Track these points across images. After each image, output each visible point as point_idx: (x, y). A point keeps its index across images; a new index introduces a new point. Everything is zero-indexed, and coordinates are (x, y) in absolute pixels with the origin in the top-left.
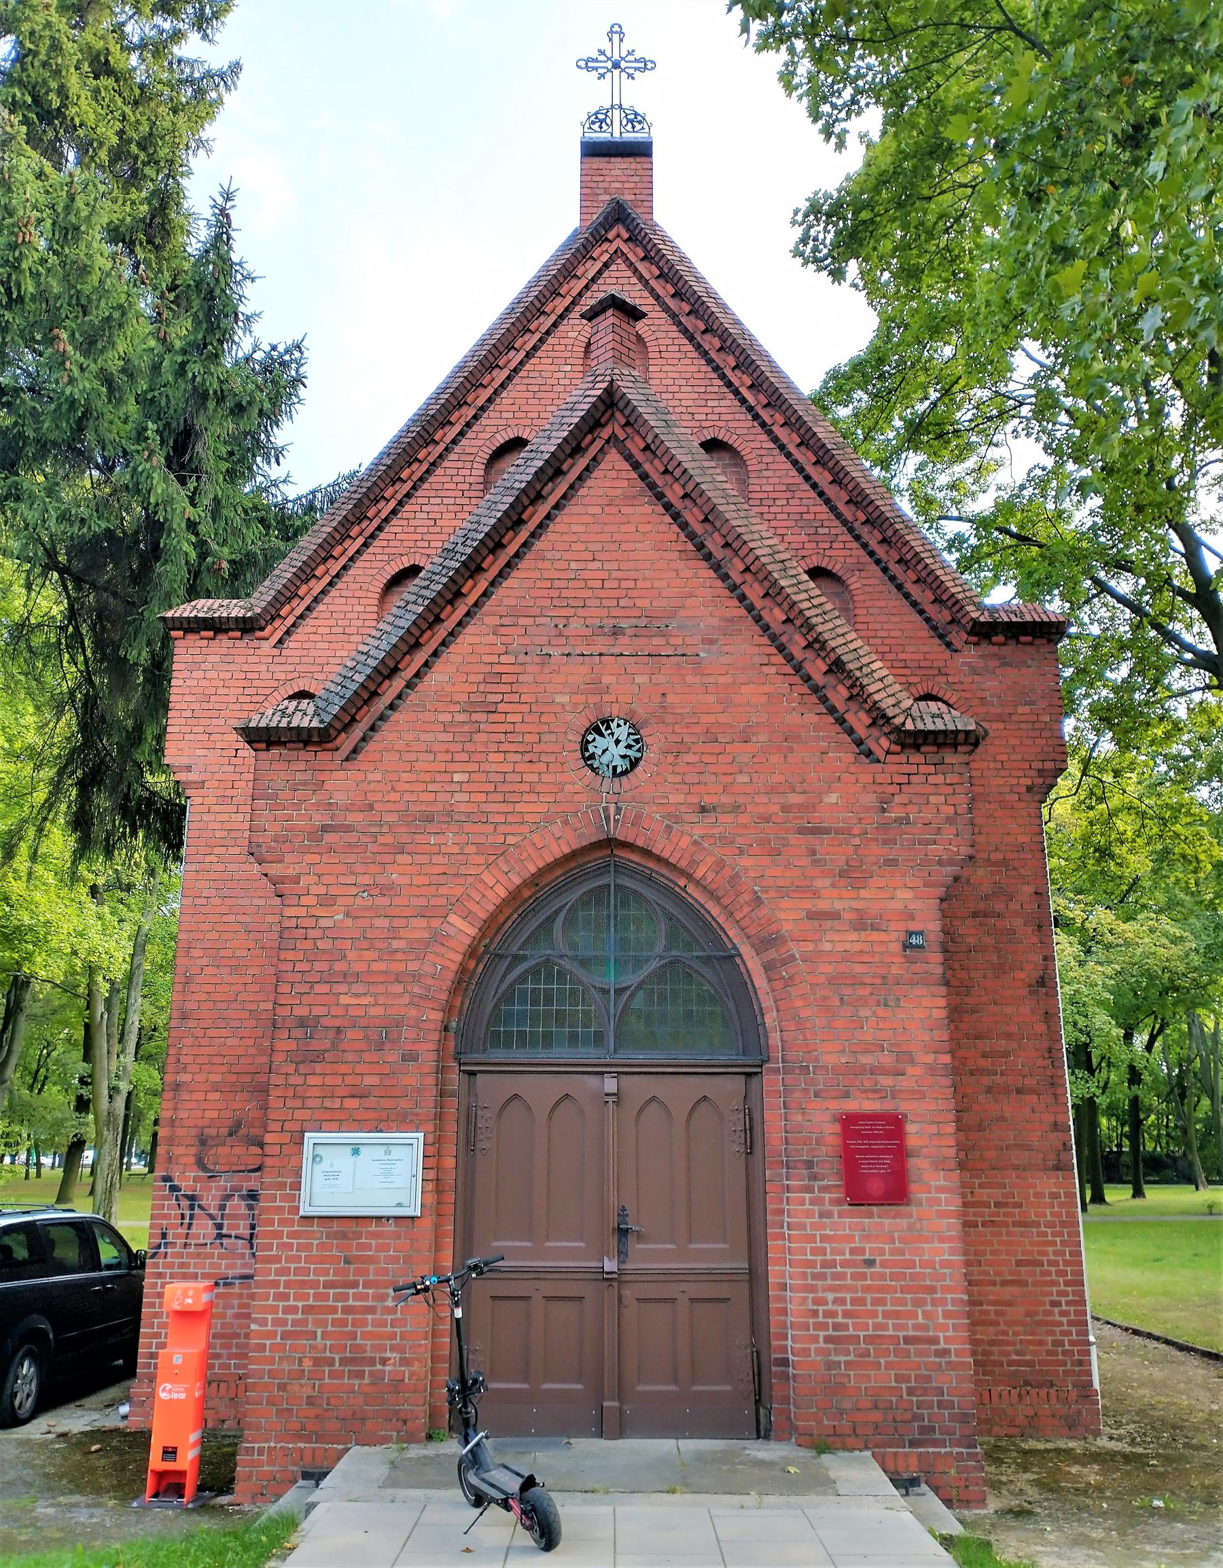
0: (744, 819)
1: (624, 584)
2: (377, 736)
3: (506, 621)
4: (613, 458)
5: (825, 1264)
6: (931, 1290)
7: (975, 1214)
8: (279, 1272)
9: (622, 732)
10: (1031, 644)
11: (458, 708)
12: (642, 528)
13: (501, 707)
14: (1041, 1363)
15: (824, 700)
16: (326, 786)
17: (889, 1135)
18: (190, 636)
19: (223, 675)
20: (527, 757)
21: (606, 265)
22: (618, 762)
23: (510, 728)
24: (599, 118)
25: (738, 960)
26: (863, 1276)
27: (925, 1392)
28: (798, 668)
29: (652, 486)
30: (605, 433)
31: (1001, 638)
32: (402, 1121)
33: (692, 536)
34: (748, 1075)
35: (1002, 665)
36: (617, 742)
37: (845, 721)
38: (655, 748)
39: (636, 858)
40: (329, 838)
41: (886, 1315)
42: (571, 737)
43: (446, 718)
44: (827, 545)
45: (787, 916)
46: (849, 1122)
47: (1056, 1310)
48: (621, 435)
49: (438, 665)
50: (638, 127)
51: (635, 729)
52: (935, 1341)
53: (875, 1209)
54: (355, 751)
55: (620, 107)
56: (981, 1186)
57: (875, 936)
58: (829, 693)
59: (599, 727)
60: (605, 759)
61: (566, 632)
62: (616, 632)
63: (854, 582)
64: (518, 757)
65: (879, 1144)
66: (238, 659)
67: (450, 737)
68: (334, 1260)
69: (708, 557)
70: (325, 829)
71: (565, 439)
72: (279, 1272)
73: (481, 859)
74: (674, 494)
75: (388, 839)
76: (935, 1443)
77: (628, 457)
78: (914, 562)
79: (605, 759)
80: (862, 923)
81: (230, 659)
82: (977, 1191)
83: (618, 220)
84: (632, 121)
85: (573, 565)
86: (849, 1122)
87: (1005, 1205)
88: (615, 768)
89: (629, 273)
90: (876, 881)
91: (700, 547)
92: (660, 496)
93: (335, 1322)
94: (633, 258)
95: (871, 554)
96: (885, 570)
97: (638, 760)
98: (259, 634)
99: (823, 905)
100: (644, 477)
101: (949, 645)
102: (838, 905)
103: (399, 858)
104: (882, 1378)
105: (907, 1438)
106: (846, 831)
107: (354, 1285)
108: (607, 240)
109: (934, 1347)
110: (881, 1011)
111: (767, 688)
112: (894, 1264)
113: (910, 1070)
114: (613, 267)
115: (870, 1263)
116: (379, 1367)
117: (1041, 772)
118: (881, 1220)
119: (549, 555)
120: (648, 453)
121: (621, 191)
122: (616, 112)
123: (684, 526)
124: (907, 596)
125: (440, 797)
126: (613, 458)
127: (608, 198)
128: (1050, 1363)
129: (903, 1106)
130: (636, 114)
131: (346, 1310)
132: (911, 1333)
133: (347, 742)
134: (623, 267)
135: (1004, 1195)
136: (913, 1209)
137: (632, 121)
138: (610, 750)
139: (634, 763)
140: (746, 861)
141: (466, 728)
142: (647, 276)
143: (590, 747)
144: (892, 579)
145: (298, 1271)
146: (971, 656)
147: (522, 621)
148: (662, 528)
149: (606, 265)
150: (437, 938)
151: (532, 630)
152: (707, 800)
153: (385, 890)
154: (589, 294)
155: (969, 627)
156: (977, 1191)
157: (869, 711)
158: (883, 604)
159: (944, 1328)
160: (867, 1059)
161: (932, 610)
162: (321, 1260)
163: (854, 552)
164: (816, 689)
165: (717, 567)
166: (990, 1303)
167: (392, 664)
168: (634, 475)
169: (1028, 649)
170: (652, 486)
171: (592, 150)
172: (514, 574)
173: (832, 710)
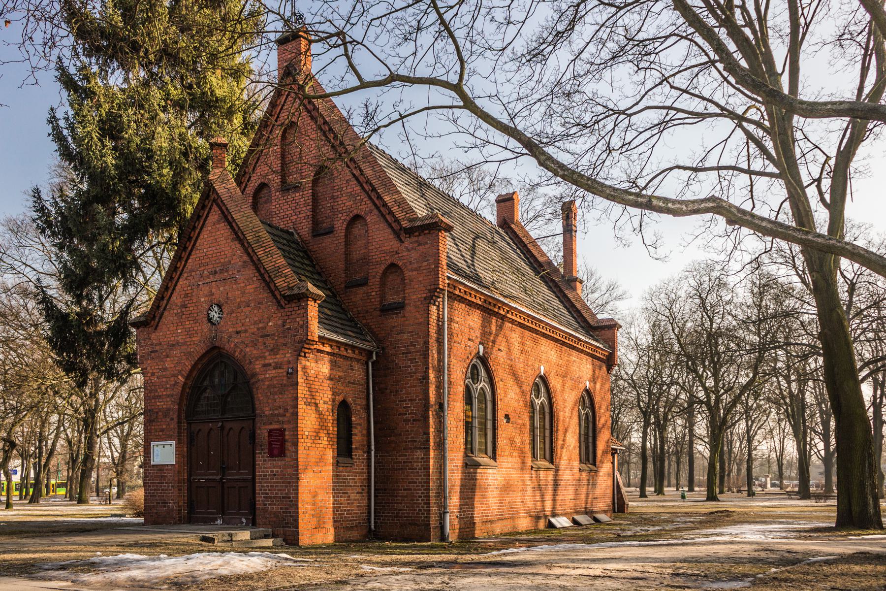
0: (247, 335)
6: (289, 483)
9: (216, 309)
31: (417, 234)
32: (168, 438)
40: (153, 355)
46: (270, 432)
62: (216, 272)
63: (368, 219)
70: (151, 352)
80: (277, 366)
86: (270, 432)
90: (281, 352)
99: (267, 362)
104: (276, 508)
106: (273, 335)
113: (288, 415)
115: (275, 475)
117: (430, 291)
140: (248, 349)
150: (176, 383)
152: (239, 329)
153: (165, 369)
160: (276, 412)
169: (429, 236)
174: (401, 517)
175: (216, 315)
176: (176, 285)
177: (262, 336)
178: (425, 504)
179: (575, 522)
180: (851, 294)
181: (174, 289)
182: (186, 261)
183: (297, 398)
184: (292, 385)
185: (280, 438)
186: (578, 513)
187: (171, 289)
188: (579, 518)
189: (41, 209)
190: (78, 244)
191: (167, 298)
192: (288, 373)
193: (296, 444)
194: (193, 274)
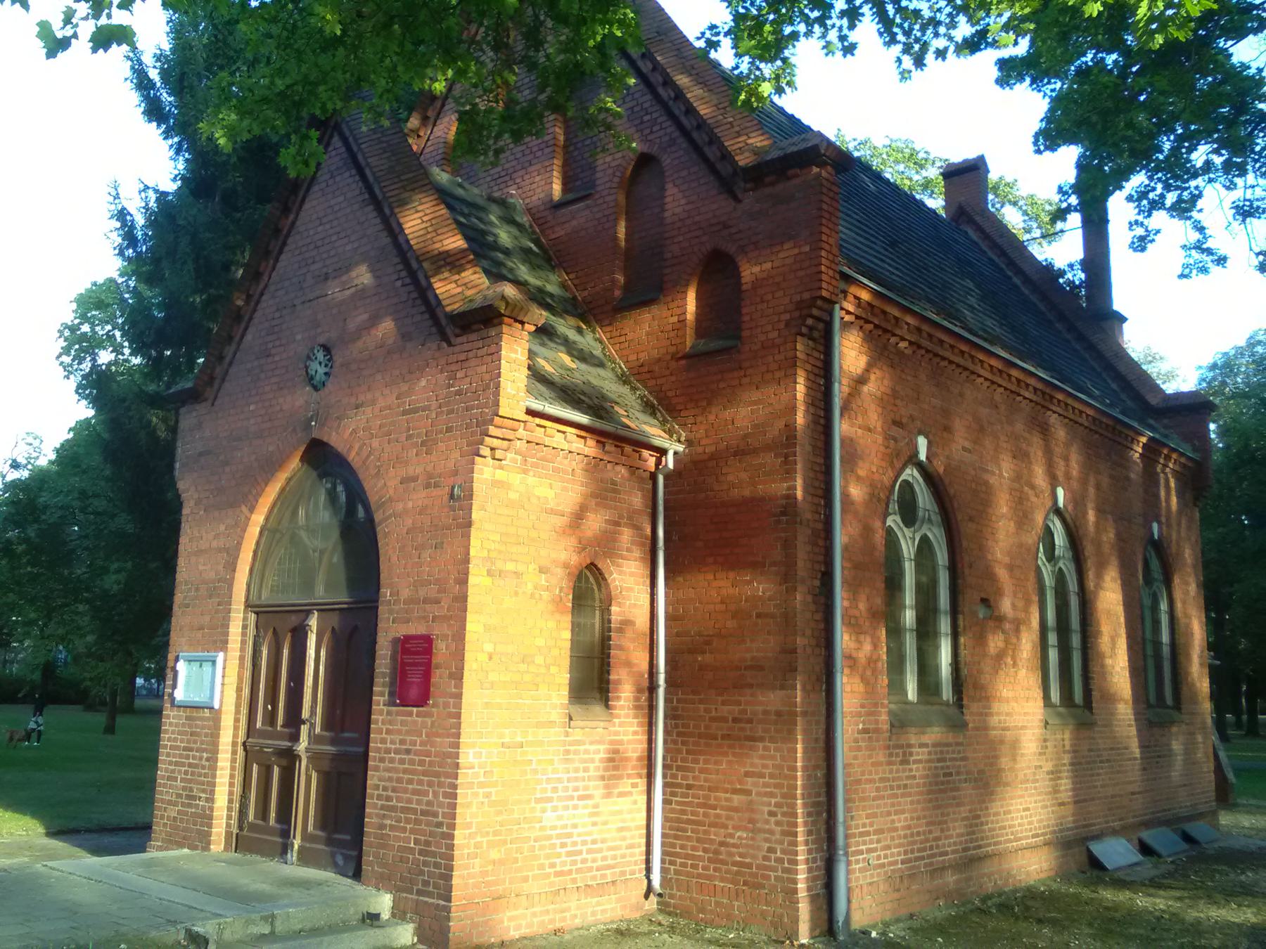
9: (320, 355)
47: (773, 819)
53: (415, 709)
56: (723, 703)
115: (408, 752)
166: (722, 808)
174: (723, 862)
176: (255, 310)
177: (405, 413)
178: (784, 833)
179: (1145, 849)
181: (251, 319)
183: (466, 560)
184: (459, 526)
186: (1147, 825)
187: (246, 318)
188: (1147, 835)
189: (122, 215)
191: (237, 339)
192: (452, 496)
193: (458, 676)
194: (287, 283)
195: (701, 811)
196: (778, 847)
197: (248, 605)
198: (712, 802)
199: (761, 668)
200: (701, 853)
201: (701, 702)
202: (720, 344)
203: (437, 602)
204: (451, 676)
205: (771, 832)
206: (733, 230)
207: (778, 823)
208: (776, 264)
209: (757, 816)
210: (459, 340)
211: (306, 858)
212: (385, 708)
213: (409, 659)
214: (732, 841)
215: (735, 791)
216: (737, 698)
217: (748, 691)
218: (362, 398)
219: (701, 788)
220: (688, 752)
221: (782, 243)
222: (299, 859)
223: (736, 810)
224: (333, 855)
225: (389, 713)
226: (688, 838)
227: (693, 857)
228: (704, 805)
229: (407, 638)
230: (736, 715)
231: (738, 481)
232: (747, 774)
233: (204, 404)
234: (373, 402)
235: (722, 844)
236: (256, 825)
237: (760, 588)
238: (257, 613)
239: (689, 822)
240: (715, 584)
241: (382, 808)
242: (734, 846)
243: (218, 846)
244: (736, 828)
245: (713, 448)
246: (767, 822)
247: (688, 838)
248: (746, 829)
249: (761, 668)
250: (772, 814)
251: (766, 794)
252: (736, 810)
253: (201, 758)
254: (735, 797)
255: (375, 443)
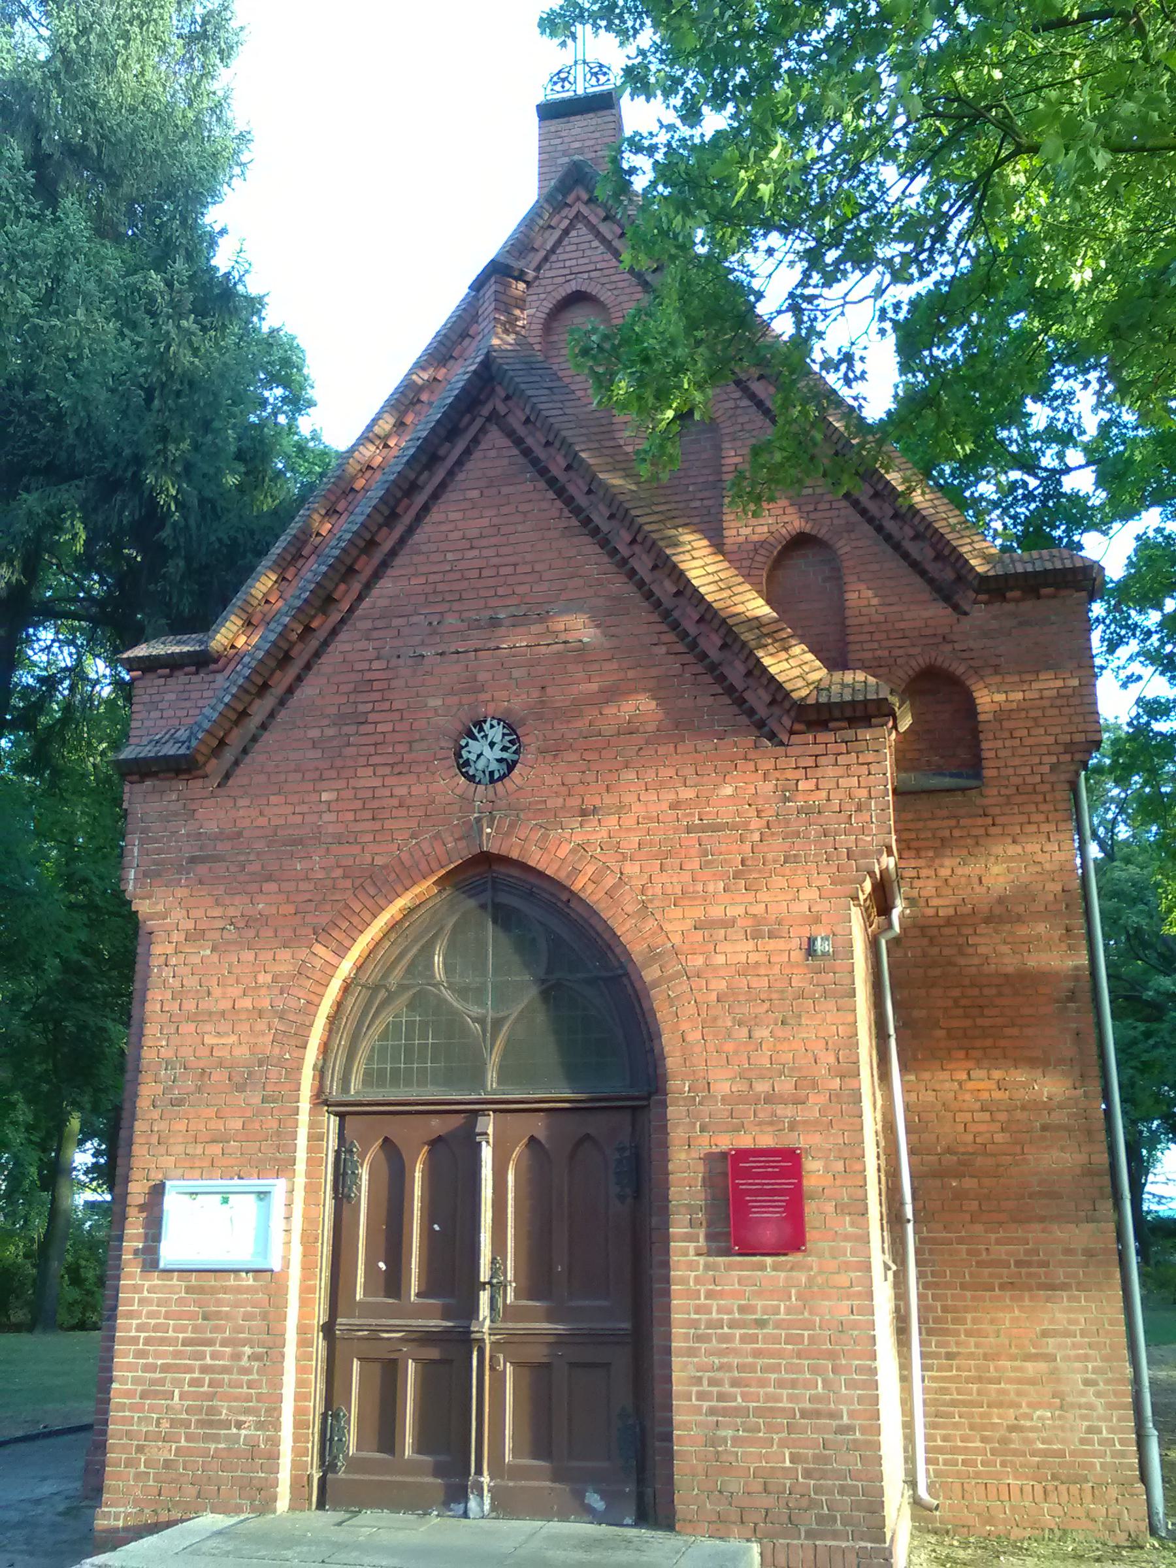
1: (503, 571)
2: (248, 759)
3: (379, 624)
4: (495, 437)
5: (710, 1324)
7: (991, 1275)
8: (139, 1329)
9: (496, 733)
10: (1054, 597)
11: (326, 722)
12: (523, 507)
13: (372, 717)
14: (1073, 1454)
15: (721, 678)
16: (197, 815)
17: (783, 1173)
18: (149, 676)
19: (180, 713)
20: (396, 770)
21: (566, 232)
22: (494, 766)
23: (380, 738)
24: (560, 78)
25: (625, 980)
26: (754, 1339)
27: (824, 1475)
28: (693, 646)
29: (535, 462)
30: (486, 411)
33: (577, 511)
34: (634, 1109)
35: (1020, 624)
36: (492, 745)
37: (745, 701)
38: (533, 748)
39: (515, 872)
41: (780, 1384)
42: (443, 744)
43: (314, 733)
44: (811, 508)
45: (678, 924)
47: (1091, 1390)
48: (502, 409)
49: (311, 677)
50: (603, 79)
51: (511, 728)
52: (834, 1415)
53: (769, 1260)
54: (227, 776)
55: (584, 62)
56: (998, 1242)
57: (772, 945)
58: (727, 671)
59: (474, 728)
60: (481, 765)
61: (442, 629)
63: (843, 547)
64: (387, 770)
65: (769, 1184)
66: (194, 695)
67: (319, 754)
68: (191, 1316)
69: (595, 532)
71: (438, 421)
72: (139, 1329)
73: (348, 883)
74: (557, 467)
75: (255, 867)
76: (835, 1535)
77: (510, 433)
78: (910, 515)
79: (481, 765)
81: (186, 695)
82: (994, 1248)
83: (577, 182)
84: (595, 74)
85: (450, 556)
87: (1029, 1264)
88: (492, 773)
89: (591, 237)
91: (587, 521)
92: (543, 472)
93: (194, 1383)
94: (594, 220)
95: (863, 512)
96: (879, 529)
97: (515, 763)
98: (213, 667)
99: (716, 912)
100: (527, 452)
101: (956, 607)
102: (735, 911)
103: (265, 886)
105: (803, 1529)
107: (210, 1343)
108: (567, 205)
109: (834, 1423)
110: (779, 1033)
111: (654, 672)
112: (790, 1324)
114: (573, 233)
115: (761, 1324)
116: (234, 1431)
118: (770, 1270)
119: (424, 548)
120: (529, 426)
121: (580, 151)
122: (580, 67)
123: (569, 501)
124: (905, 556)
125: (309, 818)
126: (495, 437)
127: (566, 160)
128: (1086, 1454)
129: (799, 1141)
130: (601, 66)
131: (205, 1369)
132: (808, 1405)
133: (215, 767)
134: (584, 230)
135: (1027, 1252)
136: (811, 1259)
137: (595, 74)
138: (485, 752)
139: (511, 766)
141: (335, 743)
142: (609, 237)
143: (464, 752)
144: (888, 538)
145: (156, 1328)
146: (980, 614)
147: (396, 622)
148: (545, 505)
149: (566, 232)
151: (405, 631)
154: (548, 265)
155: (976, 583)
156: (994, 1248)
157: (766, 687)
158: (876, 567)
159: (848, 1401)
161: (932, 568)
162: (179, 1316)
163: (843, 512)
164: (712, 668)
165: (604, 543)
166: (1010, 1381)
167: (260, 682)
168: (516, 452)
170: (535, 462)
171: (550, 112)
172: (390, 572)
173: (730, 690)
174: (1015, 1453)
175: (492, 755)
180: (956, 1153)
182: (368, 586)
185: (787, 1183)
190: (624, 406)
192: (810, 951)
195: (975, 1387)
196: (1103, 1425)
197: (321, 1099)
198: (993, 1373)
199: (1053, 1195)
200: (978, 1444)
201: (961, 1241)
202: (948, 782)
203: (799, 1102)
204: (840, 1209)
205: (1090, 1407)
206: (958, 646)
207: (1098, 1395)
208: (1028, 695)
209: (1066, 1389)
210: (795, 739)
211: (505, 1506)
212: (702, 1260)
213: (744, 1184)
214: (1028, 1424)
215: (1028, 1357)
216: (1020, 1234)
217: (1038, 1226)
218: (591, 801)
219: (971, 1356)
220: (945, 1309)
221: (1037, 672)
222: (493, 1508)
223: (1032, 1382)
224: (579, 1495)
225: (707, 1267)
226: (956, 1426)
227: (966, 1450)
228: (980, 1380)
229: (743, 1154)
230: (1022, 1257)
231: (997, 952)
232: (1045, 1334)
233: (199, 783)
234: (621, 809)
235: (1012, 1429)
236: (364, 1459)
237: (1049, 1087)
238: (341, 1116)
239: (954, 1403)
240: (970, 1085)
241: (712, 1411)
242: (1033, 1429)
243: (283, 1503)
244: (1034, 1406)
245: (951, 911)
246: (1082, 1393)
247: (956, 1426)
248: (1049, 1406)
249: (1053, 1195)
250: (1087, 1383)
251: (1078, 1358)
252: (1032, 1382)
253: (237, 1357)
254: (1028, 1365)
255: (631, 869)
